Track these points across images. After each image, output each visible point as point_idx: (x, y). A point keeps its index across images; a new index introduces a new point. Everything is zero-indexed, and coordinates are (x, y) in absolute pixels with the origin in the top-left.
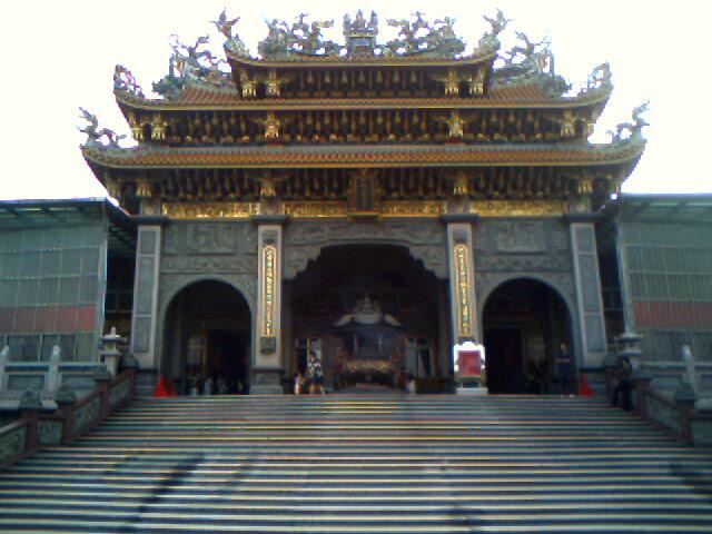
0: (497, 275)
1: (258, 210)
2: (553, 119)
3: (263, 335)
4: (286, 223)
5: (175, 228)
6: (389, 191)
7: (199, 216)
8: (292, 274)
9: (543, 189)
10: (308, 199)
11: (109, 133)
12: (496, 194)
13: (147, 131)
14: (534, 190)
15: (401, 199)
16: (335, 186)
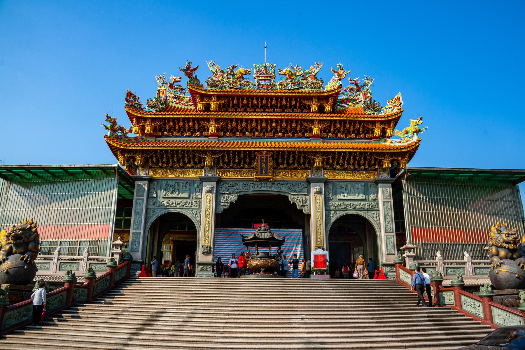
0: (338, 212)
1: (203, 173)
2: (370, 126)
3: (203, 244)
4: (219, 181)
5: (156, 183)
6: (278, 164)
7: (170, 176)
8: (221, 211)
9: (364, 165)
10: (232, 168)
11: (122, 129)
12: (338, 167)
13: (143, 129)
14: (359, 165)
15: (285, 168)
16: (247, 160)
